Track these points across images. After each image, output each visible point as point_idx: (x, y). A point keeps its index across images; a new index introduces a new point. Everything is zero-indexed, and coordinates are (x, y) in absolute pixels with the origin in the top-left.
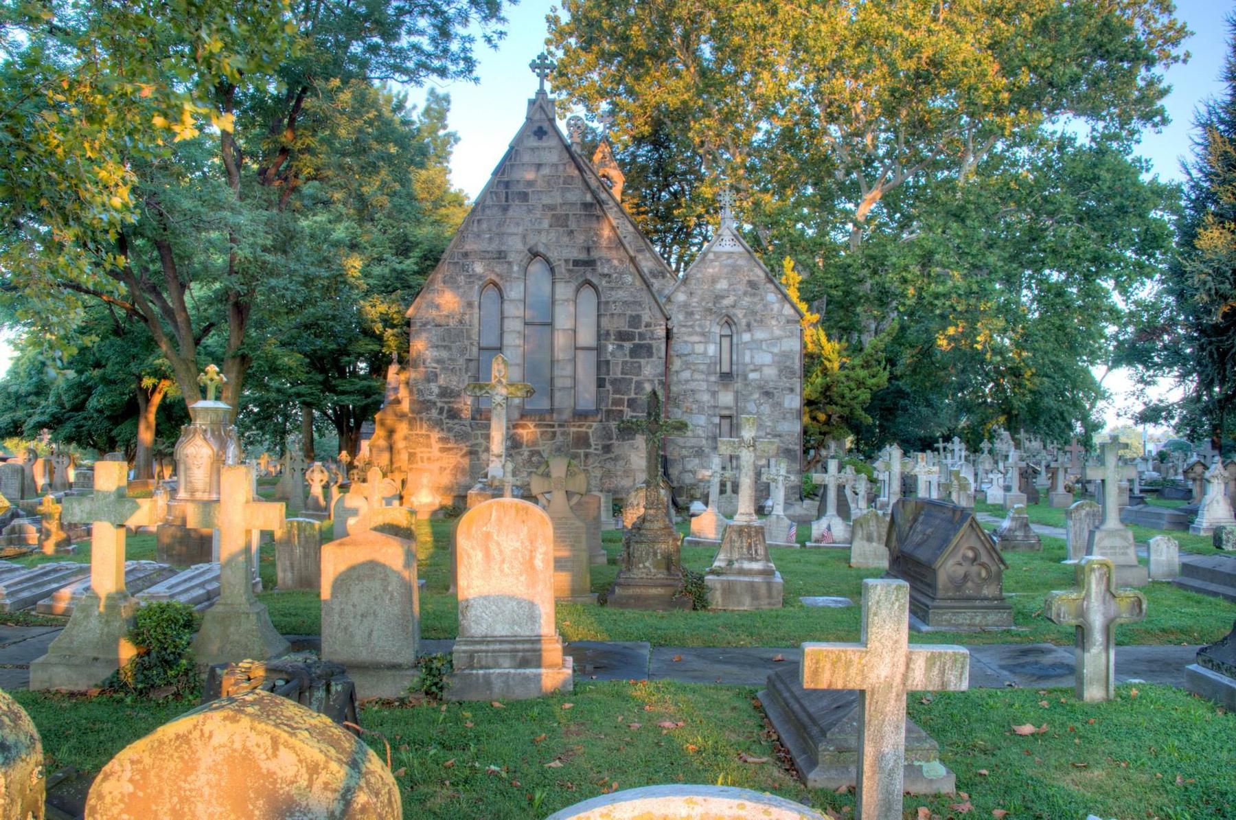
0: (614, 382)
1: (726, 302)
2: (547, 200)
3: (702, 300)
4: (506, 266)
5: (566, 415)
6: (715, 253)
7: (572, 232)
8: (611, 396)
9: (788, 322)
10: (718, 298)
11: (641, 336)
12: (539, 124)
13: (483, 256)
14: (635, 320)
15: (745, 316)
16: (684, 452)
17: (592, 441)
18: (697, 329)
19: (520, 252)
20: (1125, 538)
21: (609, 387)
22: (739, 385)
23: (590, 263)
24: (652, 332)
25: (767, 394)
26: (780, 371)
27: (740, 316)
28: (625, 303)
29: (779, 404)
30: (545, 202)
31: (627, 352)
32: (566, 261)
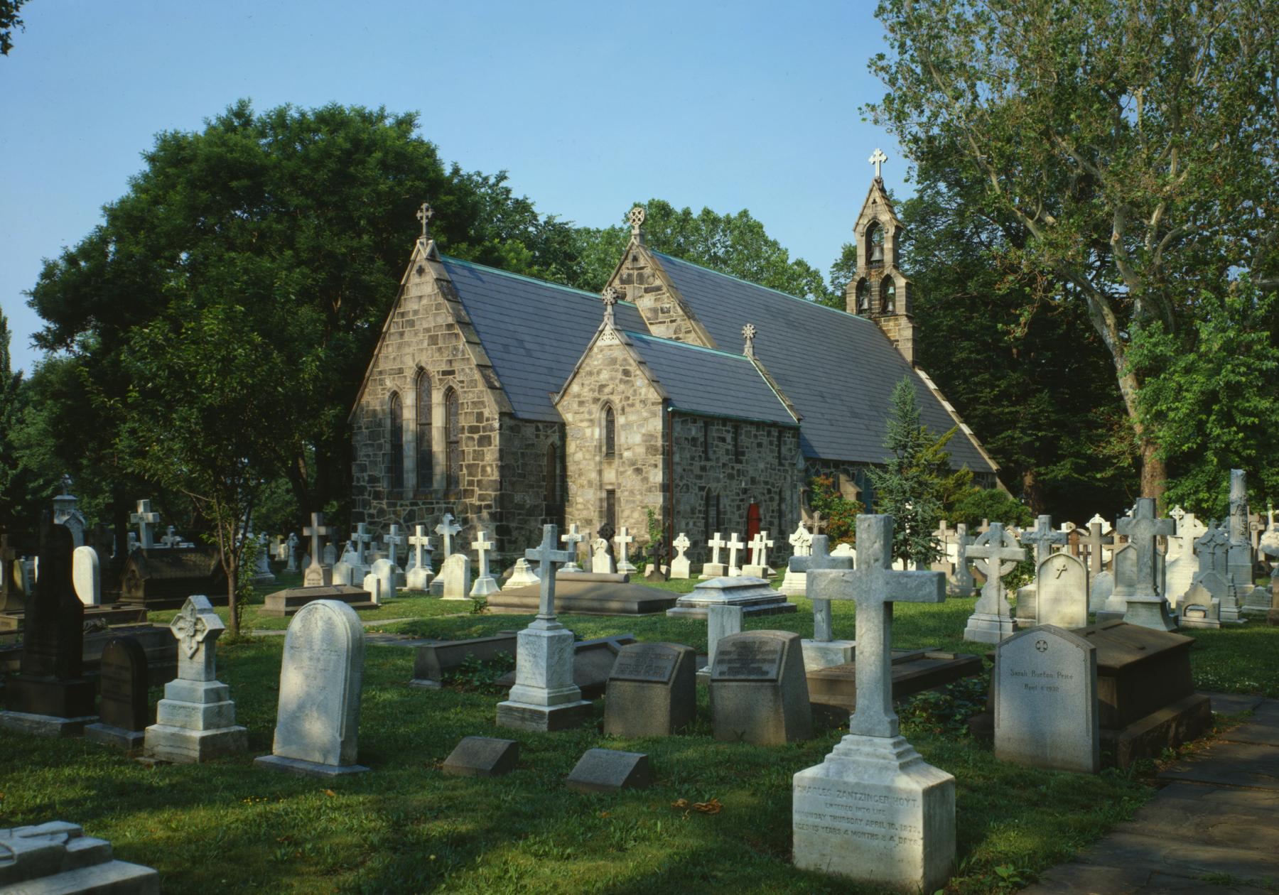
1: (607, 390)
2: (426, 325)
14: (480, 417)
27: (617, 401)
29: (645, 480)
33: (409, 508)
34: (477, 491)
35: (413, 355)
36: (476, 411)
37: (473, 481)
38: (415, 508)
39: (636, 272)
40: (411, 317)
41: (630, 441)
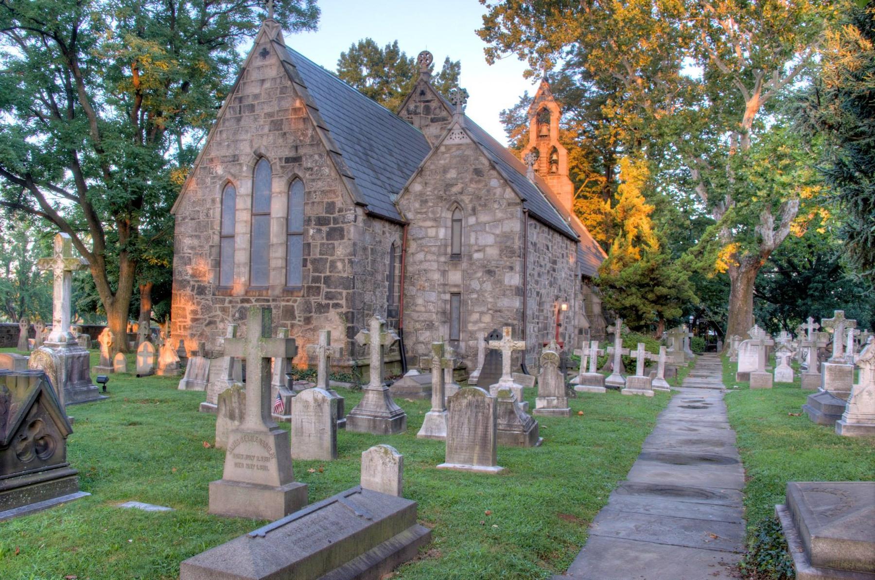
0: (314, 261)
1: (455, 190)
2: (268, 109)
3: (435, 189)
4: (238, 167)
5: (278, 292)
6: (446, 146)
7: (285, 134)
8: (311, 274)
9: (509, 204)
10: (448, 186)
11: (336, 221)
12: (264, 46)
13: (224, 160)
15: (471, 201)
16: (418, 326)
17: (296, 313)
18: (430, 215)
19: (248, 155)
20: (265, 446)
21: (310, 266)
22: (464, 265)
23: (297, 160)
24: (344, 217)
25: (490, 272)
26: (501, 251)
27: (467, 201)
28: (323, 192)
29: (500, 282)
30: (266, 111)
31: (324, 235)
32: (280, 159)
33: (239, 305)
34: (324, 289)
35: (251, 141)
36: (326, 200)
37: (319, 277)
38: (246, 305)
39: (423, 105)
40: (250, 101)
41: (482, 242)
